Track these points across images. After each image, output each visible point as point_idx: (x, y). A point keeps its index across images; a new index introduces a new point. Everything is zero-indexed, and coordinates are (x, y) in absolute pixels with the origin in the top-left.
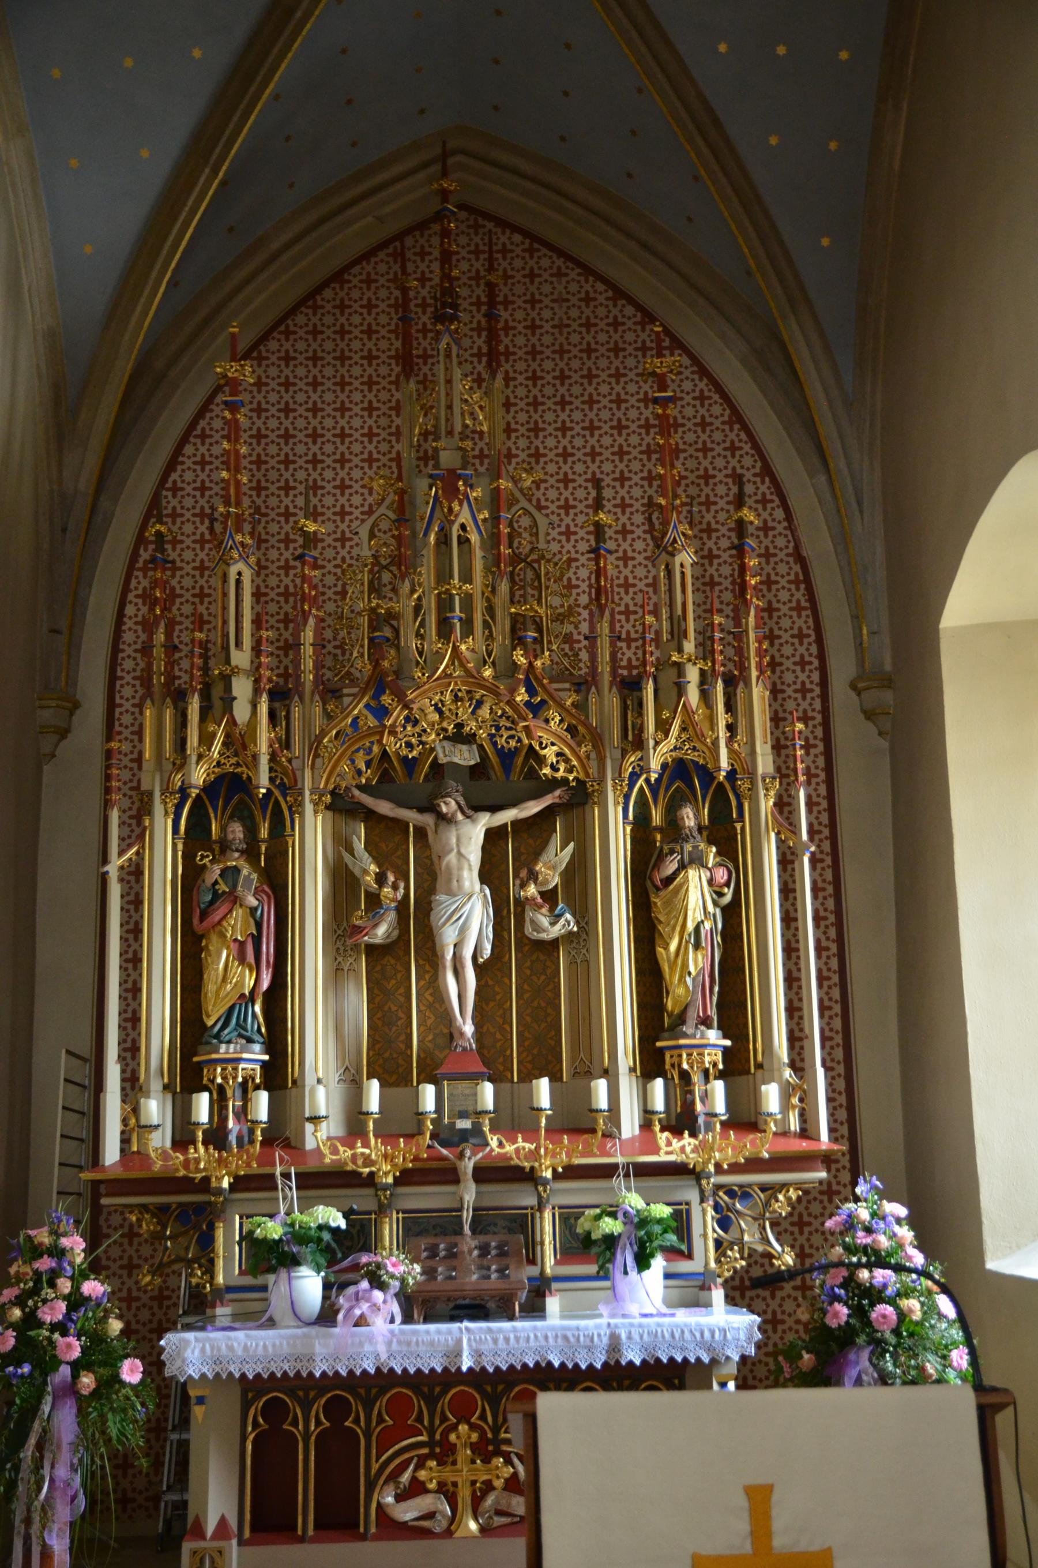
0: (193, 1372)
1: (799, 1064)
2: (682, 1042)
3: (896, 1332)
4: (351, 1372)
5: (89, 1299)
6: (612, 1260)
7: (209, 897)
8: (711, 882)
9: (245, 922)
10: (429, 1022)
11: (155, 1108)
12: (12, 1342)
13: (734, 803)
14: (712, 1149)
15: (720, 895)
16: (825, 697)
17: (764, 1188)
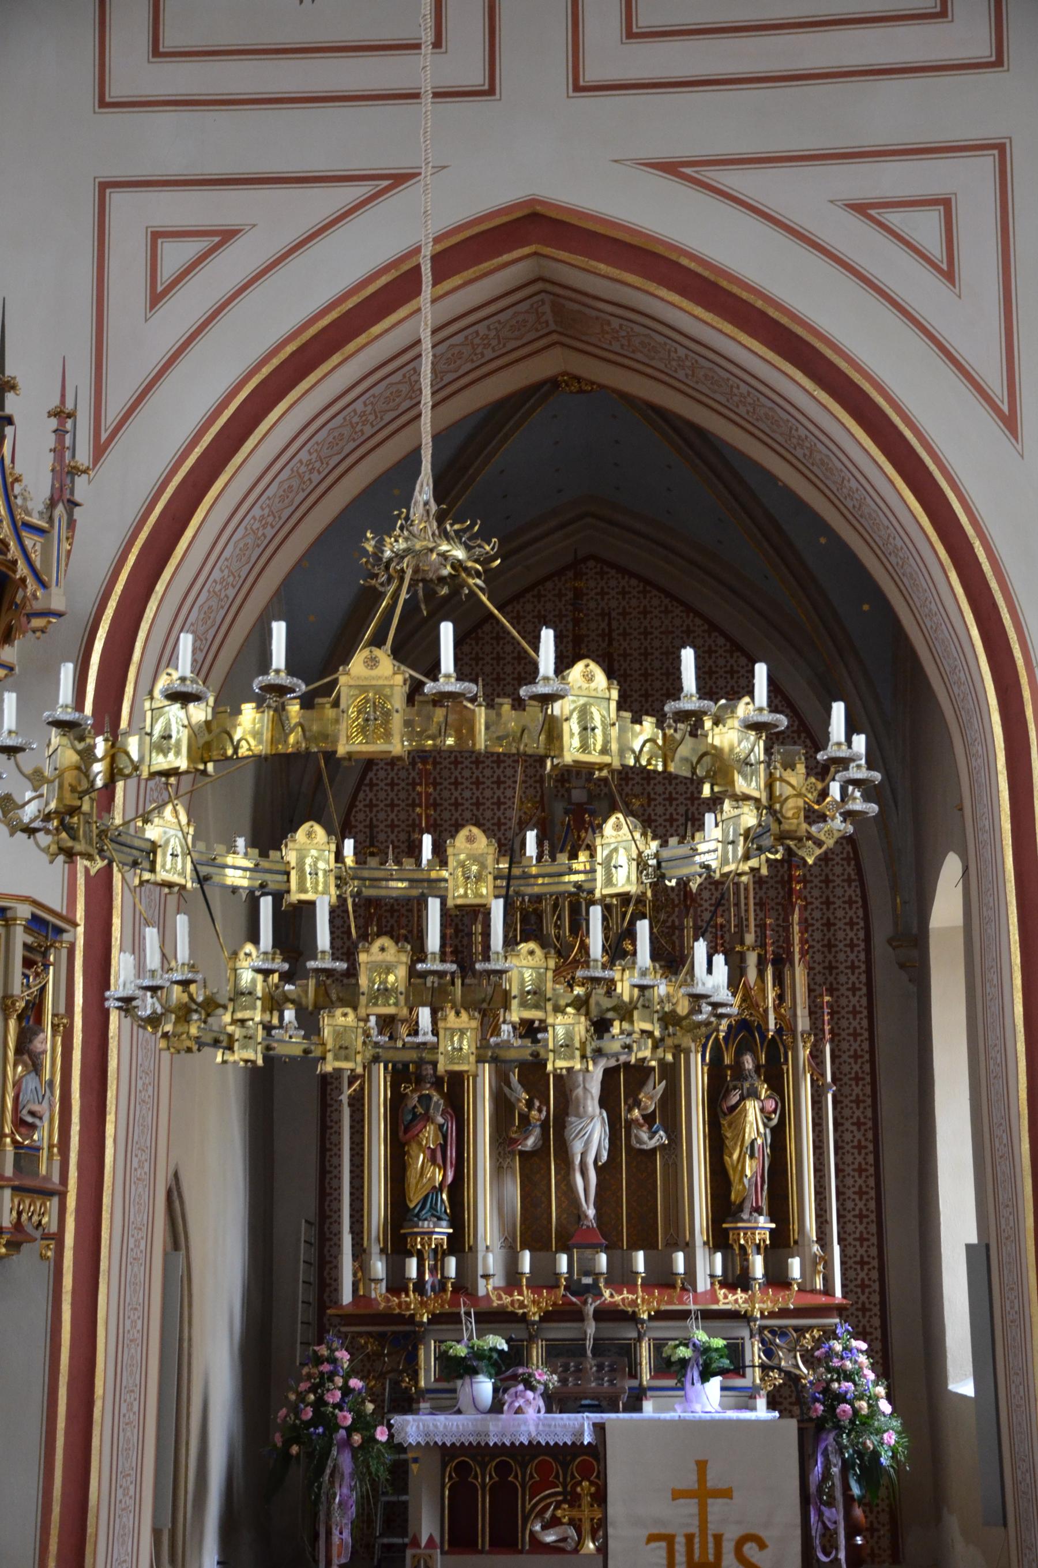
0: (412, 1440)
1: (823, 1239)
2: (740, 1225)
3: (852, 1422)
4: (513, 1444)
5: (354, 1389)
6: (684, 1376)
7: (410, 1117)
8: (762, 1110)
9: (436, 1135)
10: (564, 1205)
11: (379, 1267)
12: (311, 1414)
13: (782, 1050)
14: (760, 1303)
15: (770, 1119)
16: (868, 951)
17: (796, 1329)
